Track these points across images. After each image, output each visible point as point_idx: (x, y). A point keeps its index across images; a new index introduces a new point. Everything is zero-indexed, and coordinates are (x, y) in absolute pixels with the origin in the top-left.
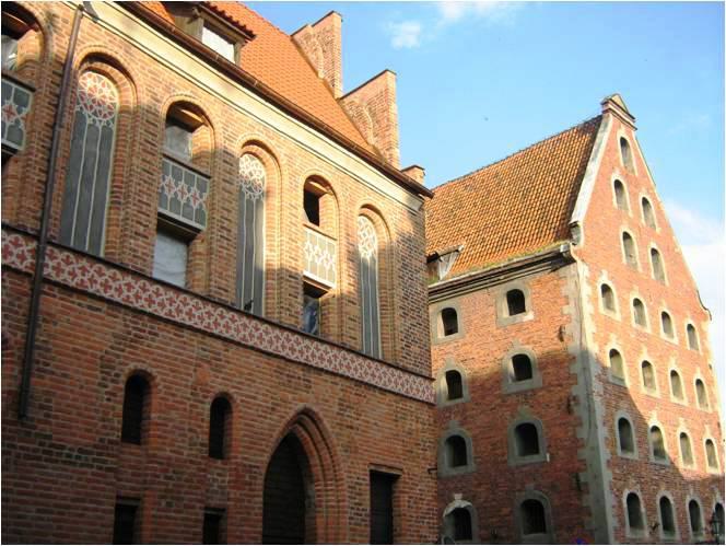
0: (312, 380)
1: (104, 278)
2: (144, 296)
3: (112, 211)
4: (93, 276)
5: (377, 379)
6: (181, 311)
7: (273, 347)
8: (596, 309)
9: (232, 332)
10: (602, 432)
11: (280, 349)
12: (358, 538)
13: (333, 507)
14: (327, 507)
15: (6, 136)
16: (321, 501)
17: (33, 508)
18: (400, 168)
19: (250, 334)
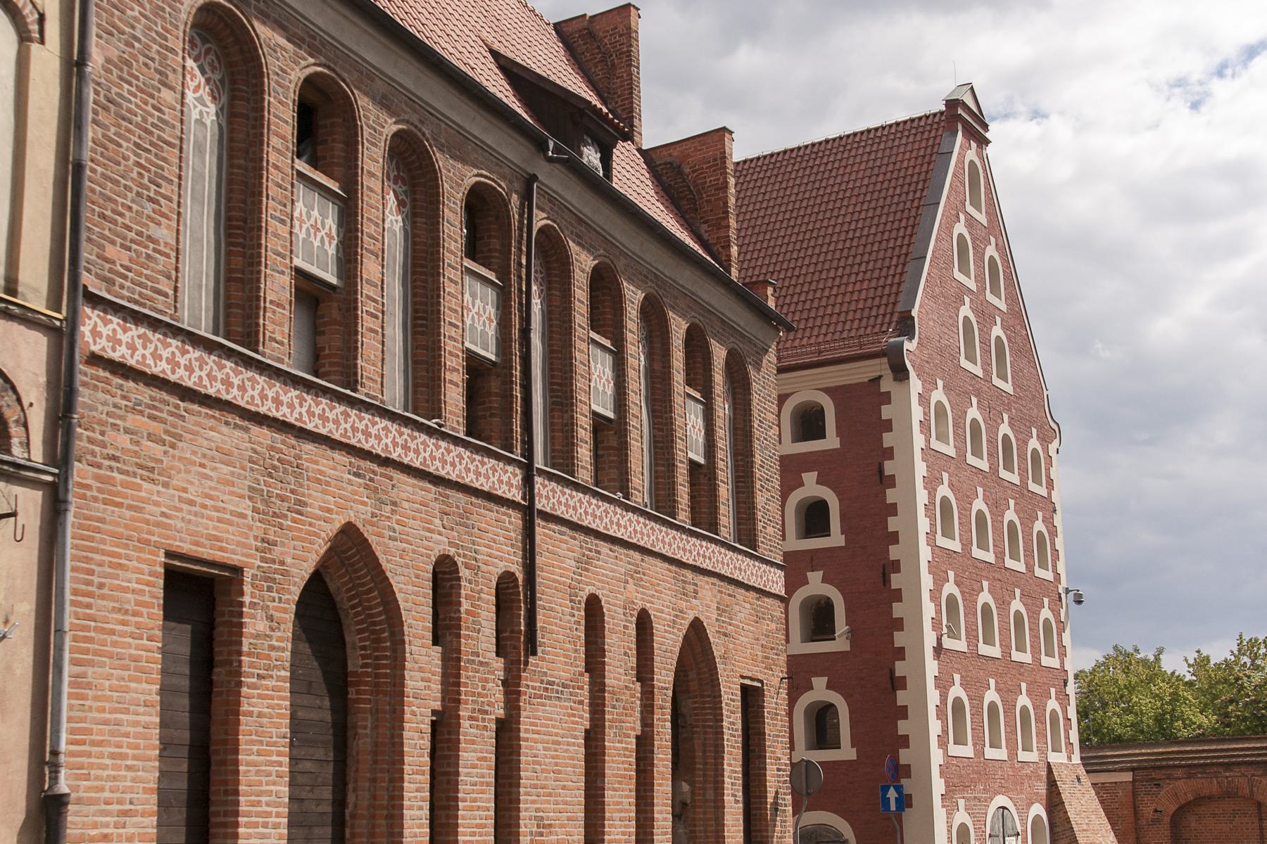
0: (699, 583)
1: (170, 350)
2: (219, 376)
3: (556, 414)
4: (96, 325)
5: (412, 454)
6: (100, 335)
7: (138, 356)
8: (927, 441)
9: (235, 391)
10: (929, 610)
11: (306, 418)
12: (710, 794)
13: (710, 727)
14: (704, 726)
15: (831, 637)
16: (697, 721)
17: (540, 746)
18: (780, 573)
19: (352, 427)
